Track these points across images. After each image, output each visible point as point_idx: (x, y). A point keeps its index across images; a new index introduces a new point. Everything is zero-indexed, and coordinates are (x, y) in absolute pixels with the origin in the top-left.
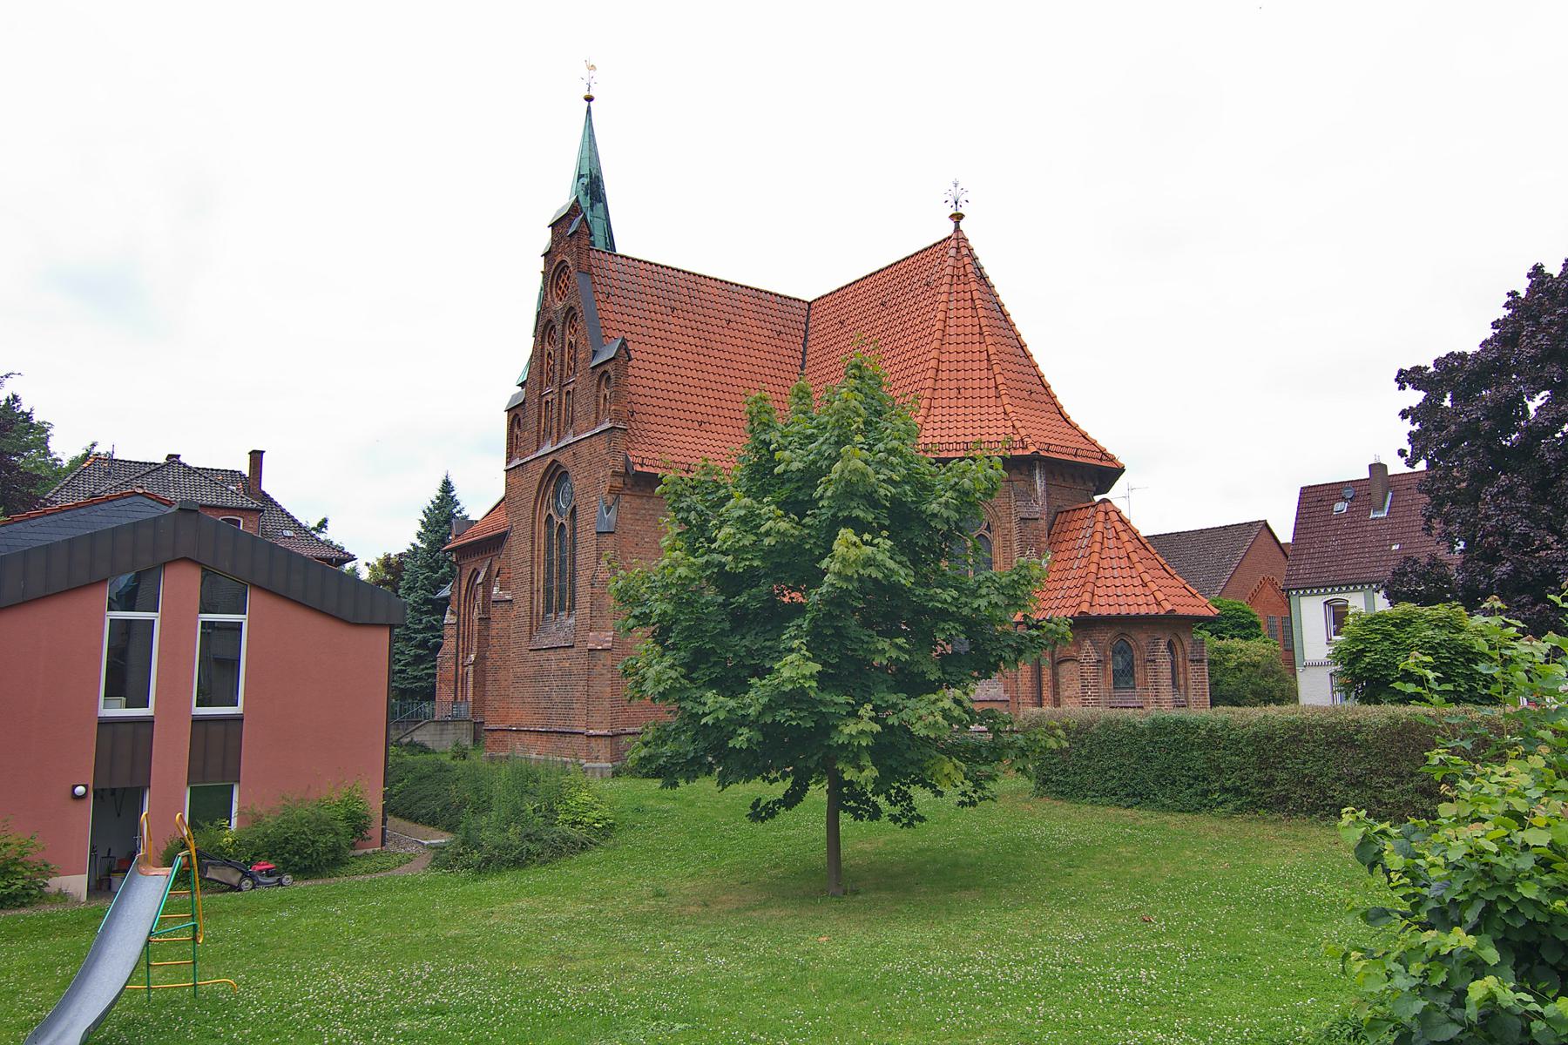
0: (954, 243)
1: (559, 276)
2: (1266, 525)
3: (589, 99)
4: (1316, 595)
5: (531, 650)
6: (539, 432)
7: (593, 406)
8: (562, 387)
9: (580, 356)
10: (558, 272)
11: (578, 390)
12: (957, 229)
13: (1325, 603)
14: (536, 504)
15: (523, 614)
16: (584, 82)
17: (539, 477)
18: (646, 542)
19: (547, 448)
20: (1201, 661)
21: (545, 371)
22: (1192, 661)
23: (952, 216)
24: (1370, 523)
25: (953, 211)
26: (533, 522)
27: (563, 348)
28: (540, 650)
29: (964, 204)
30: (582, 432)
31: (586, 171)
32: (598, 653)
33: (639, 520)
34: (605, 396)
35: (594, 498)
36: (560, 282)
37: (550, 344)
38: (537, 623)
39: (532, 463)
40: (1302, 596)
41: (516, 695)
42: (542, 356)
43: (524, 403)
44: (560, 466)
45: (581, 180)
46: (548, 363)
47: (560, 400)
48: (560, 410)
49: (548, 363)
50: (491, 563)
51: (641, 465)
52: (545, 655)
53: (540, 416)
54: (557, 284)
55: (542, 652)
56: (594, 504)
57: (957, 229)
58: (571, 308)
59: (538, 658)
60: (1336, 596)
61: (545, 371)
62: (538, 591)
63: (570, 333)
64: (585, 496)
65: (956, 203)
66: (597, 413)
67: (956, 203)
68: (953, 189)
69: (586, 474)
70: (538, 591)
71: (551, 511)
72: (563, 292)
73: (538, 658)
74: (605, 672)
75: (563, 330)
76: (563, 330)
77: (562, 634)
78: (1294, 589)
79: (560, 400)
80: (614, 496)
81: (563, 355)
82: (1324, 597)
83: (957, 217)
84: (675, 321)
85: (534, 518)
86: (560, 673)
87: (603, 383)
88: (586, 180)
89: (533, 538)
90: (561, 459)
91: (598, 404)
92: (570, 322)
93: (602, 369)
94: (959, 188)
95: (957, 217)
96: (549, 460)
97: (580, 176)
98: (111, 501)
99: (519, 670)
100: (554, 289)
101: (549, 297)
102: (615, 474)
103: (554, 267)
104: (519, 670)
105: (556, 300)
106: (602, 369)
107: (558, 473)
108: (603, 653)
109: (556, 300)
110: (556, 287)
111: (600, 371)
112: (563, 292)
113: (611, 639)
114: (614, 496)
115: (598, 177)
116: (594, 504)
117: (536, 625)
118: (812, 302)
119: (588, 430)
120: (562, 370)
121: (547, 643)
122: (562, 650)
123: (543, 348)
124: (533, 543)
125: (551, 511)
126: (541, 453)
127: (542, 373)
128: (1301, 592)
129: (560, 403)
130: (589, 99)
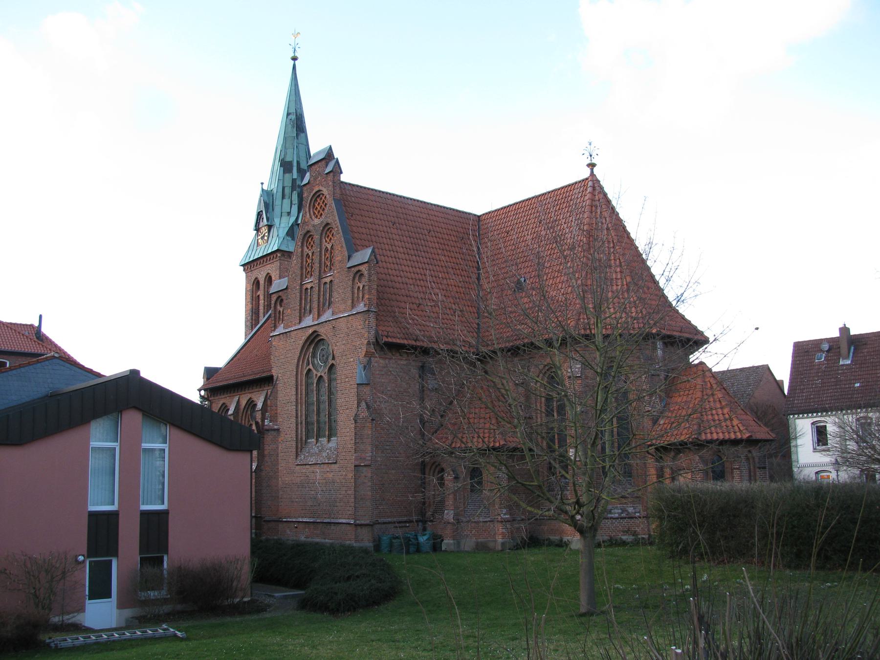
0: (590, 184)
1: (316, 200)
2: (769, 369)
3: (295, 59)
4: (806, 418)
5: (297, 465)
6: (300, 310)
7: (349, 295)
8: (320, 278)
9: (338, 259)
10: (315, 198)
11: (336, 281)
12: (592, 174)
13: (812, 424)
14: (298, 361)
15: (290, 439)
16: (291, 47)
17: (301, 343)
18: (388, 390)
19: (308, 321)
20: (764, 468)
21: (304, 267)
22: (759, 468)
23: (588, 165)
24: (840, 368)
25: (589, 162)
26: (297, 374)
27: (321, 251)
28: (305, 465)
29: (596, 157)
30: (340, 312)
31: (293, 110)
32: (361, 468)
33: (383, 375)
34: (359, 287)
35: (352, 360)
36: (316, 205)
37: (308, 248)
38: (301, 446)
39: (295, 332)
40: (797, 418)
41: (285, 497)
42: (302, 256)
43: (287, 288)
44: (318, 335)
45: (290, 117)
46: (307, 261)
47: (319, 288)
48: (319, 295)
49: (307, 261)
50: (239, 399)
51: (387, 337)
52: (311, 469)
53: (301, 299)
54: (314, 205)
55: (307, 467)
56: (352, 363)
57: (592, 174)
58: (327, 224)
59: (304, 471)
60: (822, 419)
61: (304, 267)
62: (301, 423)
63: (326, 241)
64: (344, 357)
65: (591, 156)
66: (353, 300)
67: (591, 156)
68: (589, 146)
69: (344, 342)
70: (301, 423)
71: (311, 366)
72: (319, 212)
73: (304, 471)
74: (366, 481)
75: (321, 239)
76: (321, 239)
77: (324, 454)
78: (791, 414)
79: (319, 288)
80: (368, 359)
81: (321, 257)
82: (811, 419)
83: (592, 166)
84: (395, 231)
85: (297, 372)
86: (324, 481)
87: (357, 278)
88: (293, 117)
89: (297, 386)
90: (322, 330)
91: (353, 293)
92: (326, 233)
93: (357, 269)
94: (592, 146)
95: (592, 166)
96: (310, 331)
97: (288, 114)
98: (40, 362)
99: (287, 479)
100: (312, 209)
101: (308, 215)
102: (369, 343)
103: (312, 194)
104: (287, 479)
105: (313, 217)
106: (357, 269)
107: (316, 340)
108: (365, 469)
109: (313, 217)
110: (313, 208)
111: (355, 270)
112: (319, 212)
113: (370, 458)
114: (368, 359)
115: (301, 115)
116: (352, 363)
117: (300, 446)
118: (481, 216)
119: (345, 311)
120: (320, 267)
121: (313, 460)
122: (326, 465)
123: (302, 251)
124: (297, 389)
125: (311, 366)
126: (303, 325)
127: (302, 268)
128: (796, 416)
129: (319, 290)
130: (295, 59)
